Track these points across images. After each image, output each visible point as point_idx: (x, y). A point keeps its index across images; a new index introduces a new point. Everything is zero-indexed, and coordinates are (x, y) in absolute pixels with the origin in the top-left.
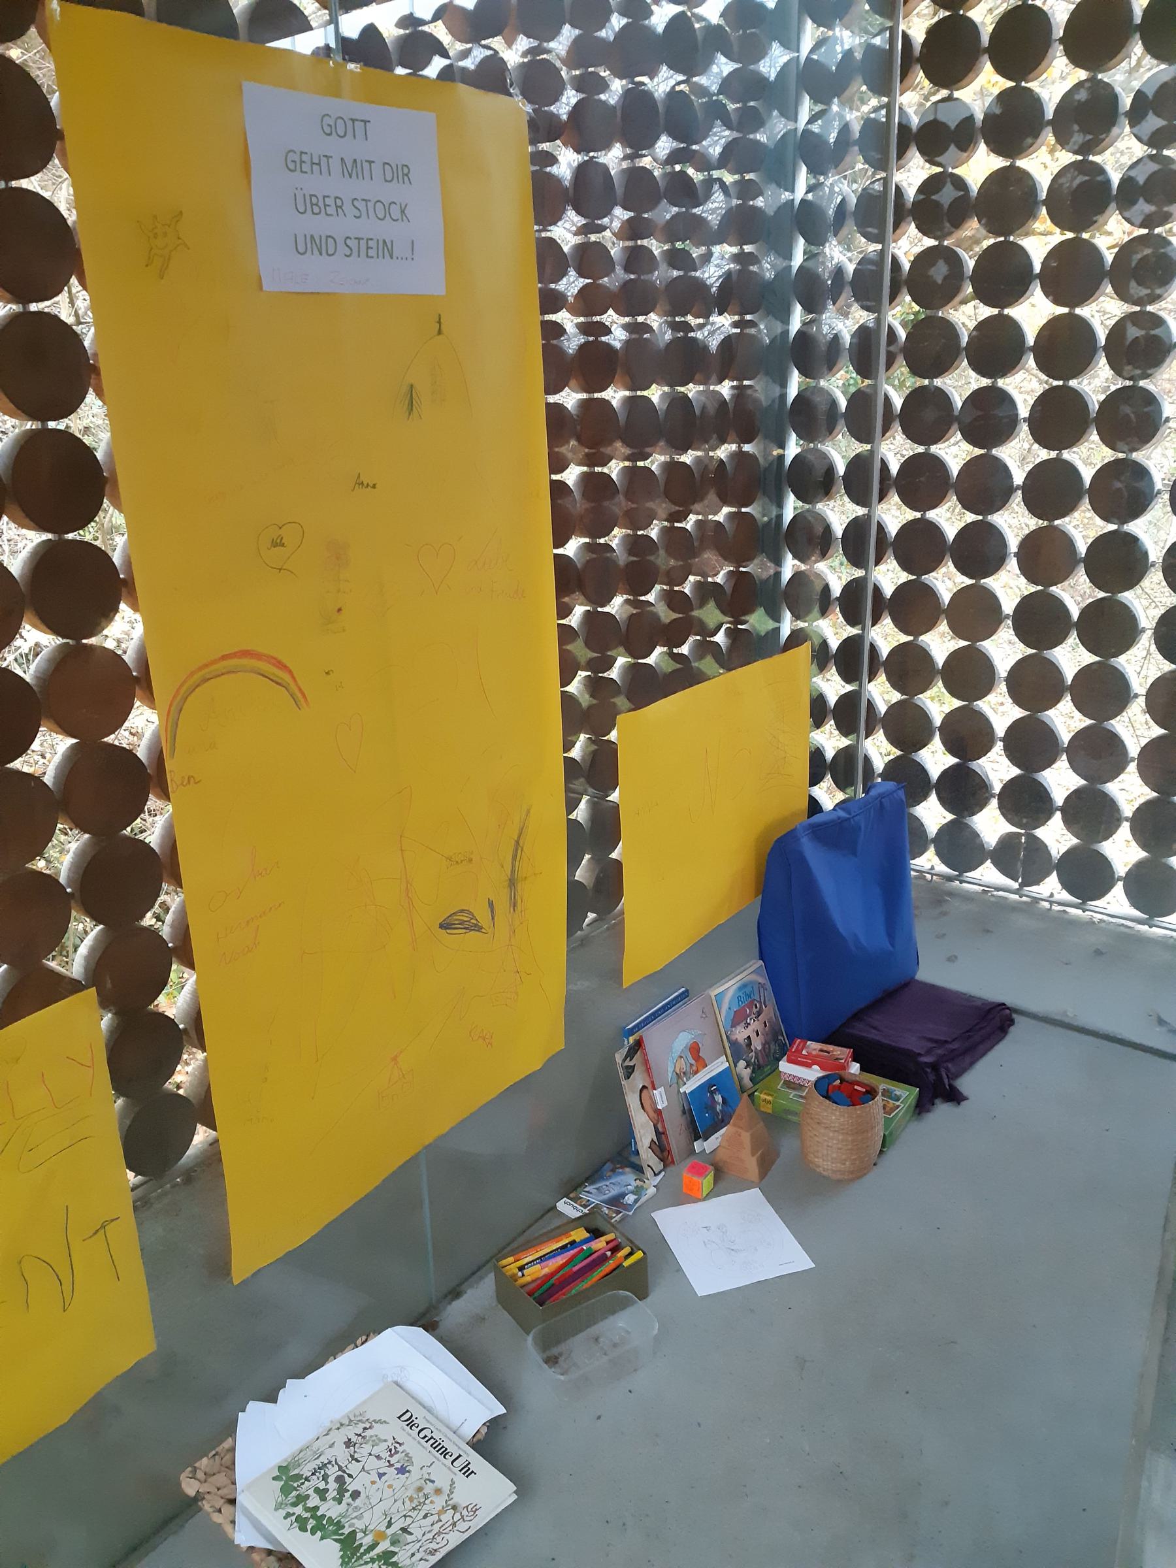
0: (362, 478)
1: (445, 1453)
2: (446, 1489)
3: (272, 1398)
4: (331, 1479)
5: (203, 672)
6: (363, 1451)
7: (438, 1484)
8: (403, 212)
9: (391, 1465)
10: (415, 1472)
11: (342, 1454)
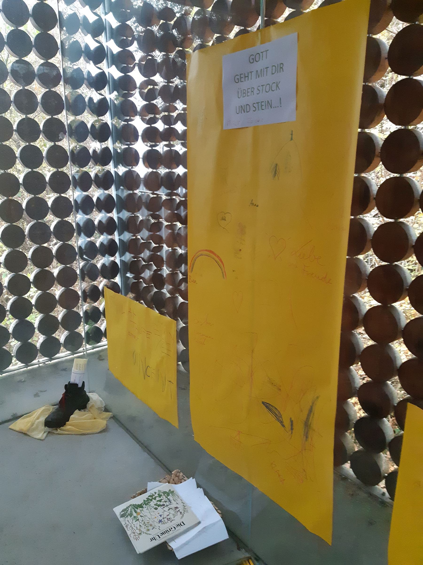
0: (253, 202)
1: (162, 534)
2: (148, 532)
3: (198, 486)
4: (164, 503)
5: (202, 252)
6: (172, 512)
7: (151, 530)
8: (277, 86)
9: (163, 518)
10: (157, 525)
11: (174, 505)
